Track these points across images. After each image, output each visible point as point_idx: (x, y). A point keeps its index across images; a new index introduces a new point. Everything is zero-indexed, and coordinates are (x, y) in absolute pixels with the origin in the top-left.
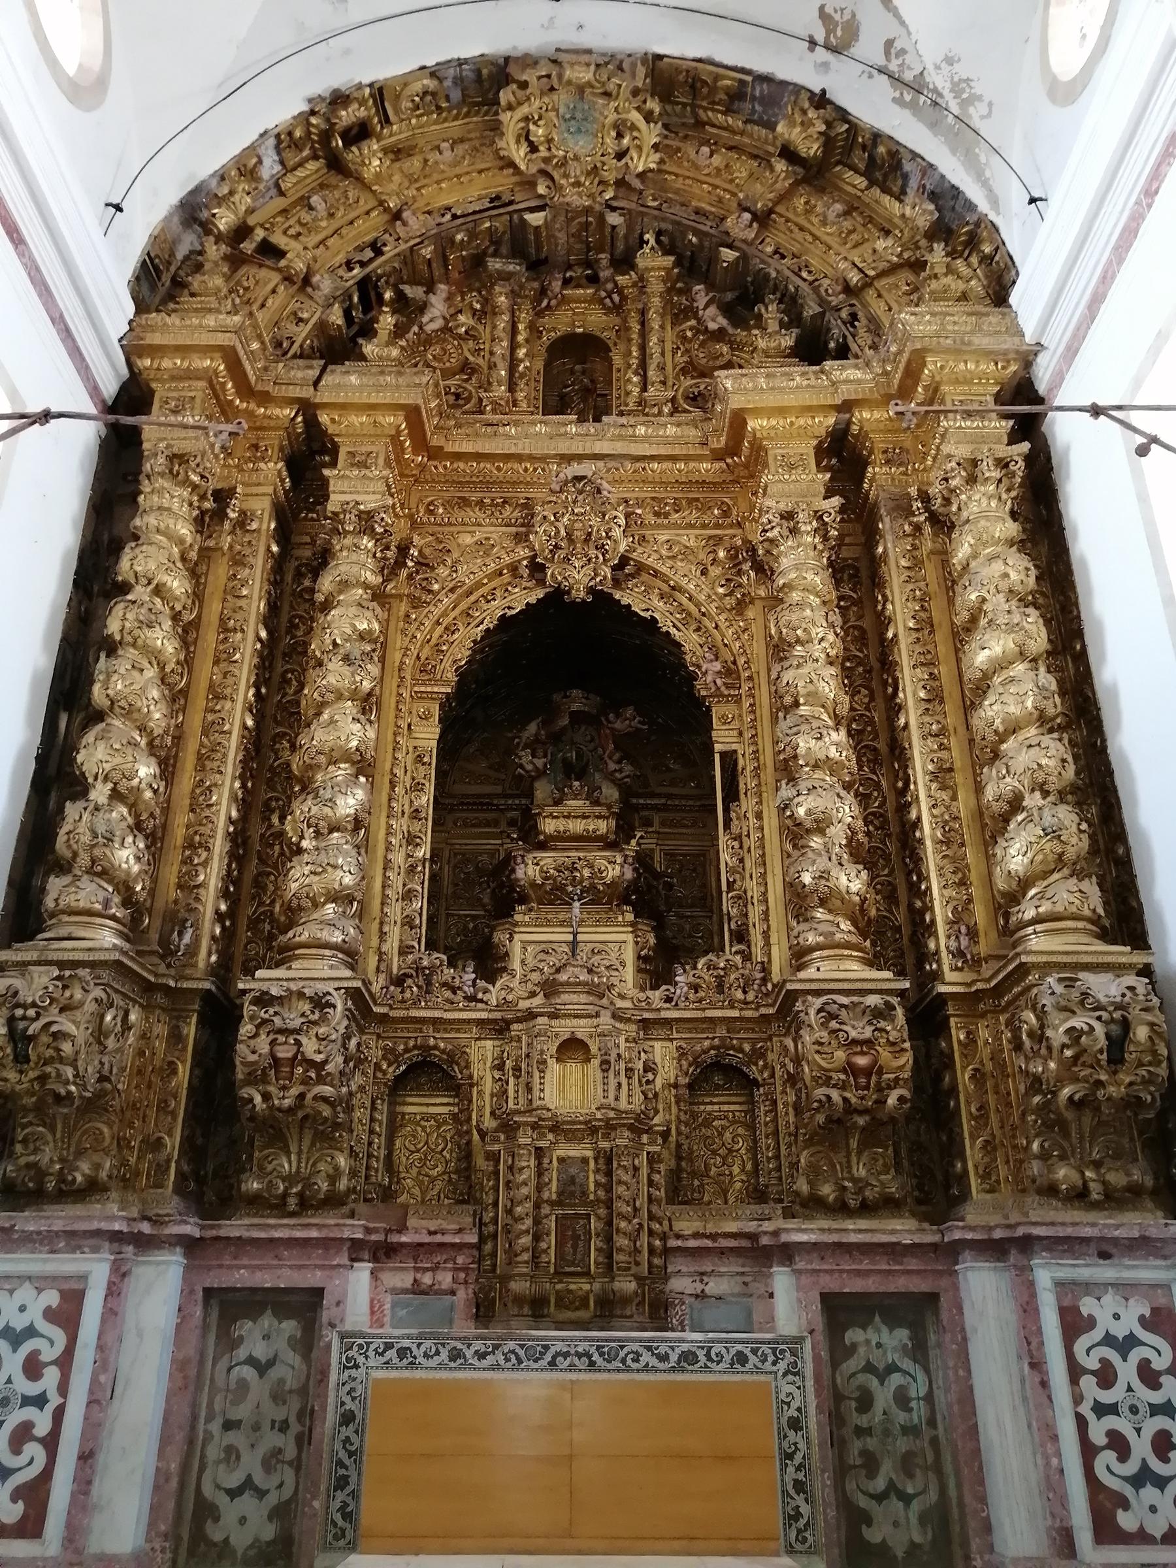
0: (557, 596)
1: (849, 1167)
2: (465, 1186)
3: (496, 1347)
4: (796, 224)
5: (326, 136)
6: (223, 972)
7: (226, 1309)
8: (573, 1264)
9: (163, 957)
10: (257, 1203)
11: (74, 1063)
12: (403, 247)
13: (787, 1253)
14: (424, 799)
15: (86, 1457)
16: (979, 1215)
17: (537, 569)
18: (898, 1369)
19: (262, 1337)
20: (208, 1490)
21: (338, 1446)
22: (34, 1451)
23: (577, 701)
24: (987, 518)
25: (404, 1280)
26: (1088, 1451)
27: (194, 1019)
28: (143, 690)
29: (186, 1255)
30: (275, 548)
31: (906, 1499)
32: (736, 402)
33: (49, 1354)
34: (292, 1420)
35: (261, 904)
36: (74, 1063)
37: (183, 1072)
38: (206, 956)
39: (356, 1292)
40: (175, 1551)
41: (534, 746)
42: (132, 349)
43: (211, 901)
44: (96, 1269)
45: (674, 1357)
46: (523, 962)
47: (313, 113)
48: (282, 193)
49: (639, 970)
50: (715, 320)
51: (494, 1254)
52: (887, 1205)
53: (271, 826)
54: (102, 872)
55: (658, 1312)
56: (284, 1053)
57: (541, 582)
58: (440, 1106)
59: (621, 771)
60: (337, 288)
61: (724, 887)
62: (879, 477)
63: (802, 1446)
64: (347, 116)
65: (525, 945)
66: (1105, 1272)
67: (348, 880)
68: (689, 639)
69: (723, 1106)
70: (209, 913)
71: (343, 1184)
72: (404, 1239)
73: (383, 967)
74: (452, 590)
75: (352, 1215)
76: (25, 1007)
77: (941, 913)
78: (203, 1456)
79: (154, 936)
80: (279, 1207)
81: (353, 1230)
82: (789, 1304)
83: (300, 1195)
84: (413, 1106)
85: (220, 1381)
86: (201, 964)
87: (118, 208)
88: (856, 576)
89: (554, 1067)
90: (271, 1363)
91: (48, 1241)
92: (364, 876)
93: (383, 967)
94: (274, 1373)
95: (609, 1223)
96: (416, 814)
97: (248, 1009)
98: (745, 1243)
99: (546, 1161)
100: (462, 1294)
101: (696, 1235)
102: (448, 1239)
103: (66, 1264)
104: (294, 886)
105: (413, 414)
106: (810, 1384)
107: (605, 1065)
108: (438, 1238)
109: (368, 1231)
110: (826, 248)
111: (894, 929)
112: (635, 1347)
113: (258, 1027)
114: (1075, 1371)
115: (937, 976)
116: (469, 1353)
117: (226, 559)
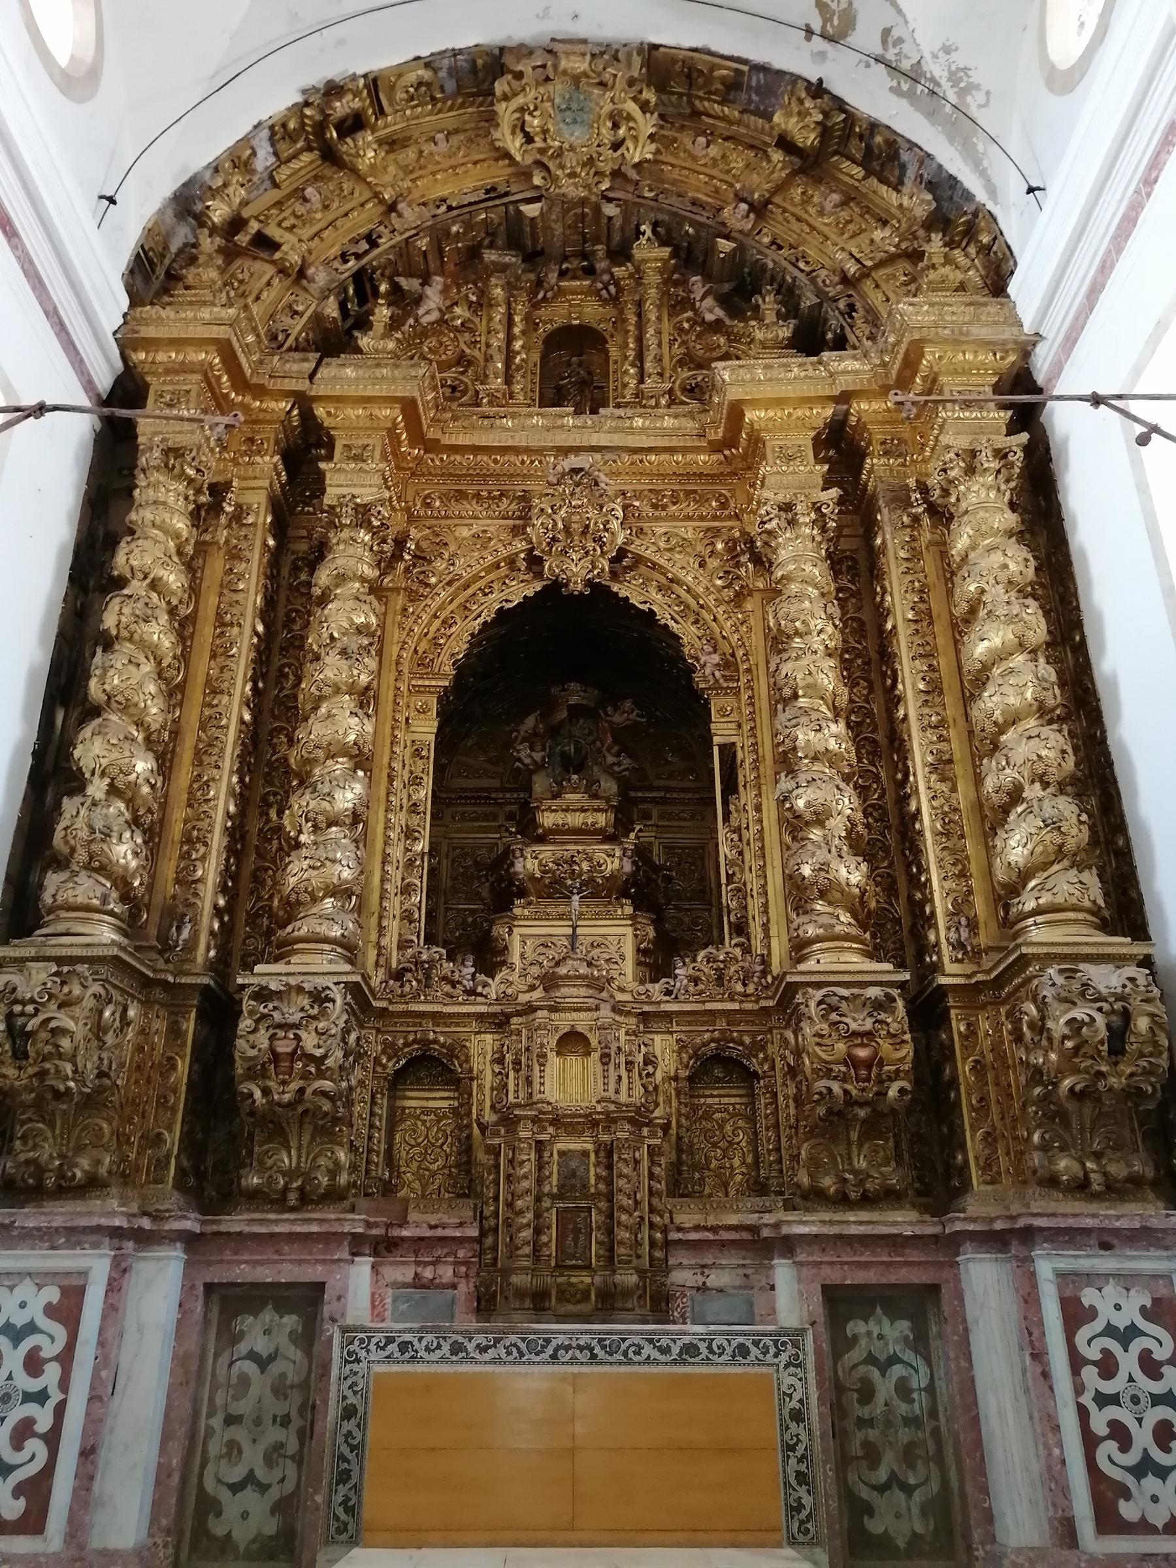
0: (555, 588)
1: (850, 1159)
2: (466, 1179)
3: (497, 1341)
4: (793, 215)
5: (320, 128)
6: (222, 967)
7: (224, 1305)
8: (574, 1257)
9: (161, 953)
10: (255, 1198)
11: (73, 1059)
12: (399, 238)
13: (788, 1245)
14: (422, 793)
15: (88, 1453)
16: (980, 1206)
17: (534, 562)
18: (900, 1361)
19: (264, 1332)
20: (210, 1485)
21: (340, 1439)
22: (36, 1446)
23: (575, 693)
24: (985, 509)
25: (405, 1274)
26: (1090, 1441)
27: (193, 1015)
28: (140, 684)
29: (186, 1251)
30: (271, 542)
31: (908, 1490)
32: (734, 394)
33: (1109, 1448)
34: (294, 1414)
35: (259, 898)
36: (73, 1059)
37: (183, 1067)
38: (205, 952)
39: (357, 1287)
40: (177, 1547)
41: (531, 740)
42: (127, 342)
43: (209, 896)
44: (97, 1265)
45: (676, 1350)
46: (522, 956)
47: (307, 104)
48: (276, 185)
49: (639, 964)
50: (712, 311)
51: (495, 1248)
52: (888, 1197)
53: (269, 820)
54: (100, 867)
55: (660, 1304)
56: (284, 1047)
57: (539, 575)
58: (440, 1100)
59: (619, 764)
60: (333, 281)
61: (723, 880)
62: (878, 468)
63: (804, 1437)
64: (341, 107)
65: (524, 939)
66: (1105, 1263)
67: (346, 874)
68: (687, 632)
69: (723, 1099)
70: (208, 908)
71: (343, 1179)
72: (405, 1233)
73: (382, 961)
74: (450, 583)
75: (352, 1210)
76: (23, 1003)
77: (941, 905)
78: (205, 1452)
79: (153, 932)
80: (279, 1202)
81: (355, 1224)
82: (790, 1295)
83: (301, 1189)
84: (414, 1100)
85: (222, 1372)
86: (200, 959)
87: (112, 200)
88: (855, 568)
89: (554, 1061)
90: (272, 1358)
91: (47, 1237)
92: (363, 870)
93: (382, 961)
94: (275, 1368)
95: (611, 1216)
96: (414, 809)
97: (247, 1004)
98: (745, 1235)
99: (546, 1154)
100: (463, 1288)
101: (697, 1228)
102: (449, 1233)
103: (65, 1260)
104: (292, 881)
105: (409, 407)
106: (812, 1375)
107: (605, 1058)
108: (439, 1232)
109: (369, 1225)
110: (824, 239)
111: (894, 921)
112: (636, 1339)
113: (257, 1022)
114: (1077, 1362)
115: (937, 968)
116: (470, 1347)
117: (222, 552)
